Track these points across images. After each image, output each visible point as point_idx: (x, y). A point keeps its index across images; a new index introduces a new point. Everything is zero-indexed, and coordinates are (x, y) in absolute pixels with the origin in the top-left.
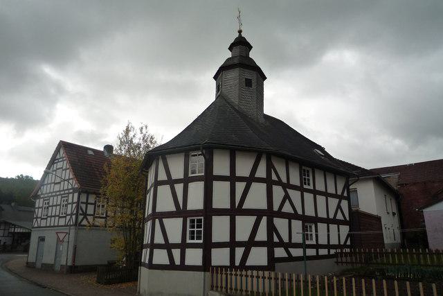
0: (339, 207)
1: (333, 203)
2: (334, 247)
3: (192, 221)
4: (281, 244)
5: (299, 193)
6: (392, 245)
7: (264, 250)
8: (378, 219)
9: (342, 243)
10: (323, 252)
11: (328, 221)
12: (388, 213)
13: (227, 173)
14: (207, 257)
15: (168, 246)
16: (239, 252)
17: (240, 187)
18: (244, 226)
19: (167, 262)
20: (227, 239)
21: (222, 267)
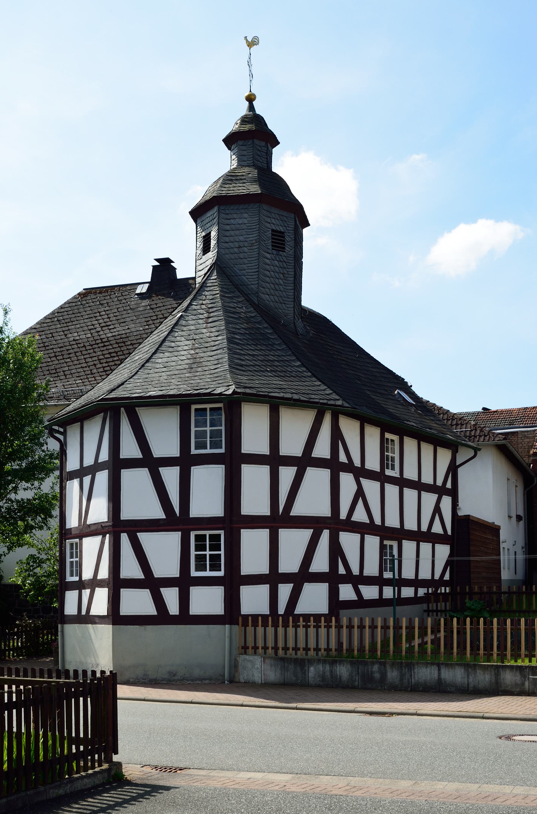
0: (437, 510)
1: (429, 500)
2: (424, 583)
3: (200, 539)
4: (349, 578)
5: (377, 485)
6: (511, 581)
7: (323, 588)
8: (495, 530)
9: (437, 576)
10: (407, 592)
11: (418, 536)
12: (510, 517)
13: (264, 449)
14: (232, 601)
15: (151, 583)
16: (285, 591)
17: (287, 474)
18: (293, 544)
19: (151, 610)
20: (264, 569)
21: (255, 617)
